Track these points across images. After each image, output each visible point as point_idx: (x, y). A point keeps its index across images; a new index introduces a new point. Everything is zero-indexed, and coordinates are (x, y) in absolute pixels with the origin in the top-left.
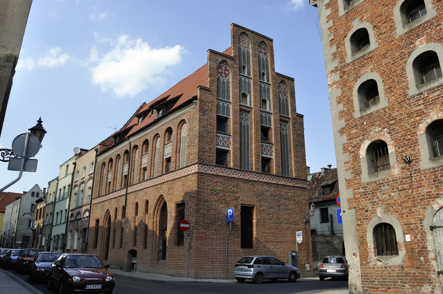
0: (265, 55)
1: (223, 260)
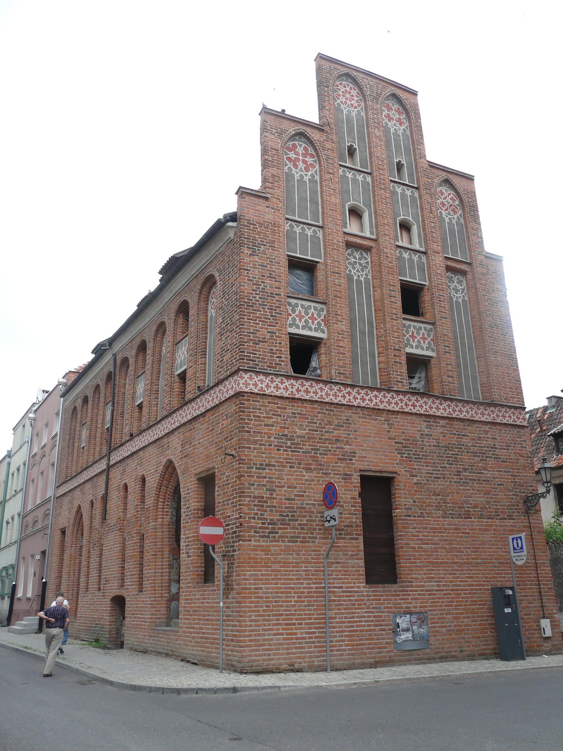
1: (319, 619)
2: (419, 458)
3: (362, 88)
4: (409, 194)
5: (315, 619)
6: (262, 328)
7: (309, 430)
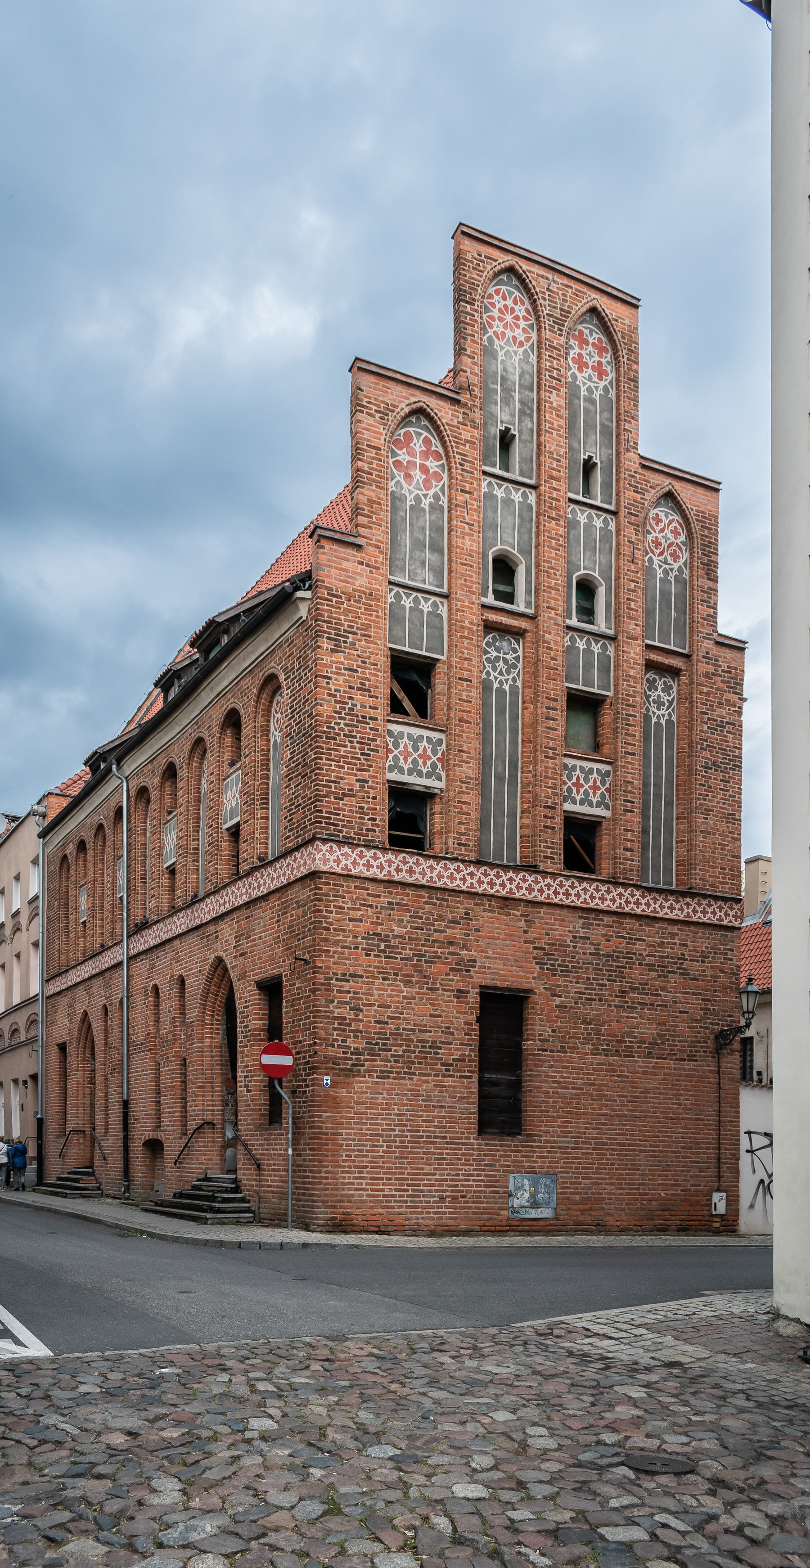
0: (601, 379)
2: (567, 971)
3: (535, 301)
4: (598, 526)
5: (408, 1174)
6: (348, 774)
7: (411, 927)
